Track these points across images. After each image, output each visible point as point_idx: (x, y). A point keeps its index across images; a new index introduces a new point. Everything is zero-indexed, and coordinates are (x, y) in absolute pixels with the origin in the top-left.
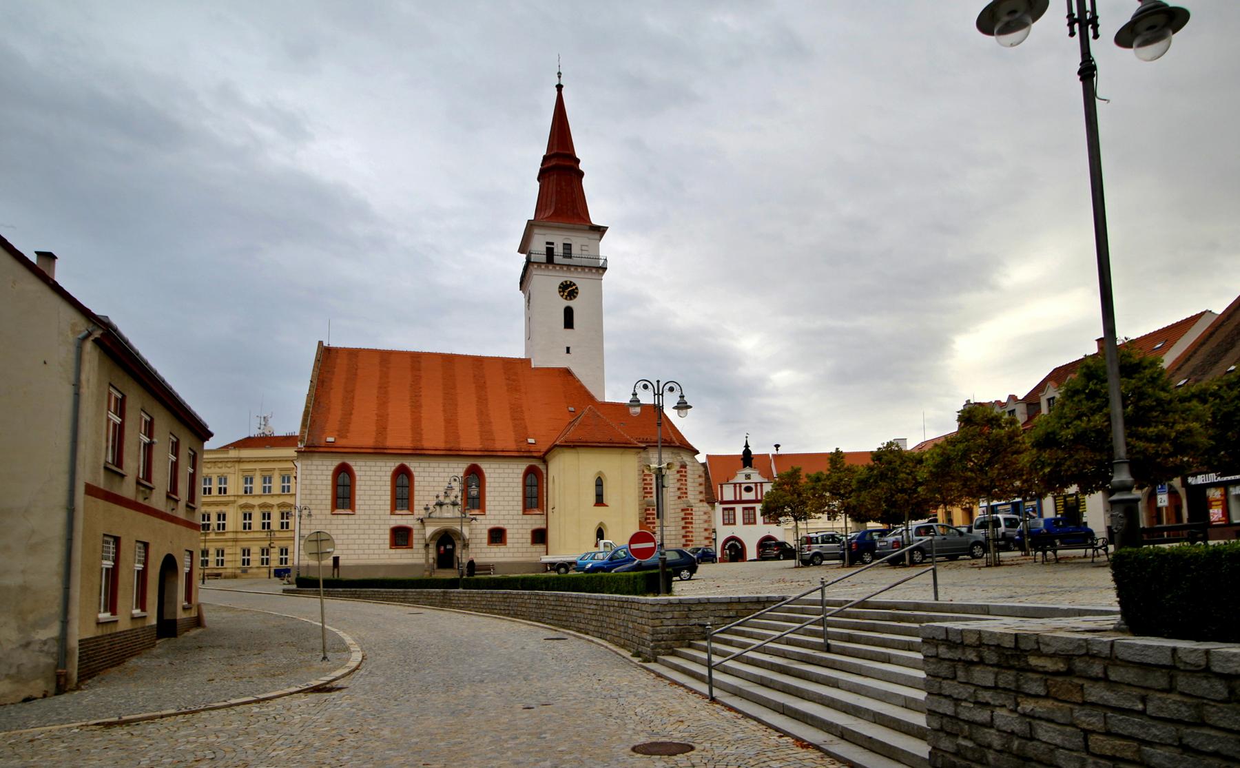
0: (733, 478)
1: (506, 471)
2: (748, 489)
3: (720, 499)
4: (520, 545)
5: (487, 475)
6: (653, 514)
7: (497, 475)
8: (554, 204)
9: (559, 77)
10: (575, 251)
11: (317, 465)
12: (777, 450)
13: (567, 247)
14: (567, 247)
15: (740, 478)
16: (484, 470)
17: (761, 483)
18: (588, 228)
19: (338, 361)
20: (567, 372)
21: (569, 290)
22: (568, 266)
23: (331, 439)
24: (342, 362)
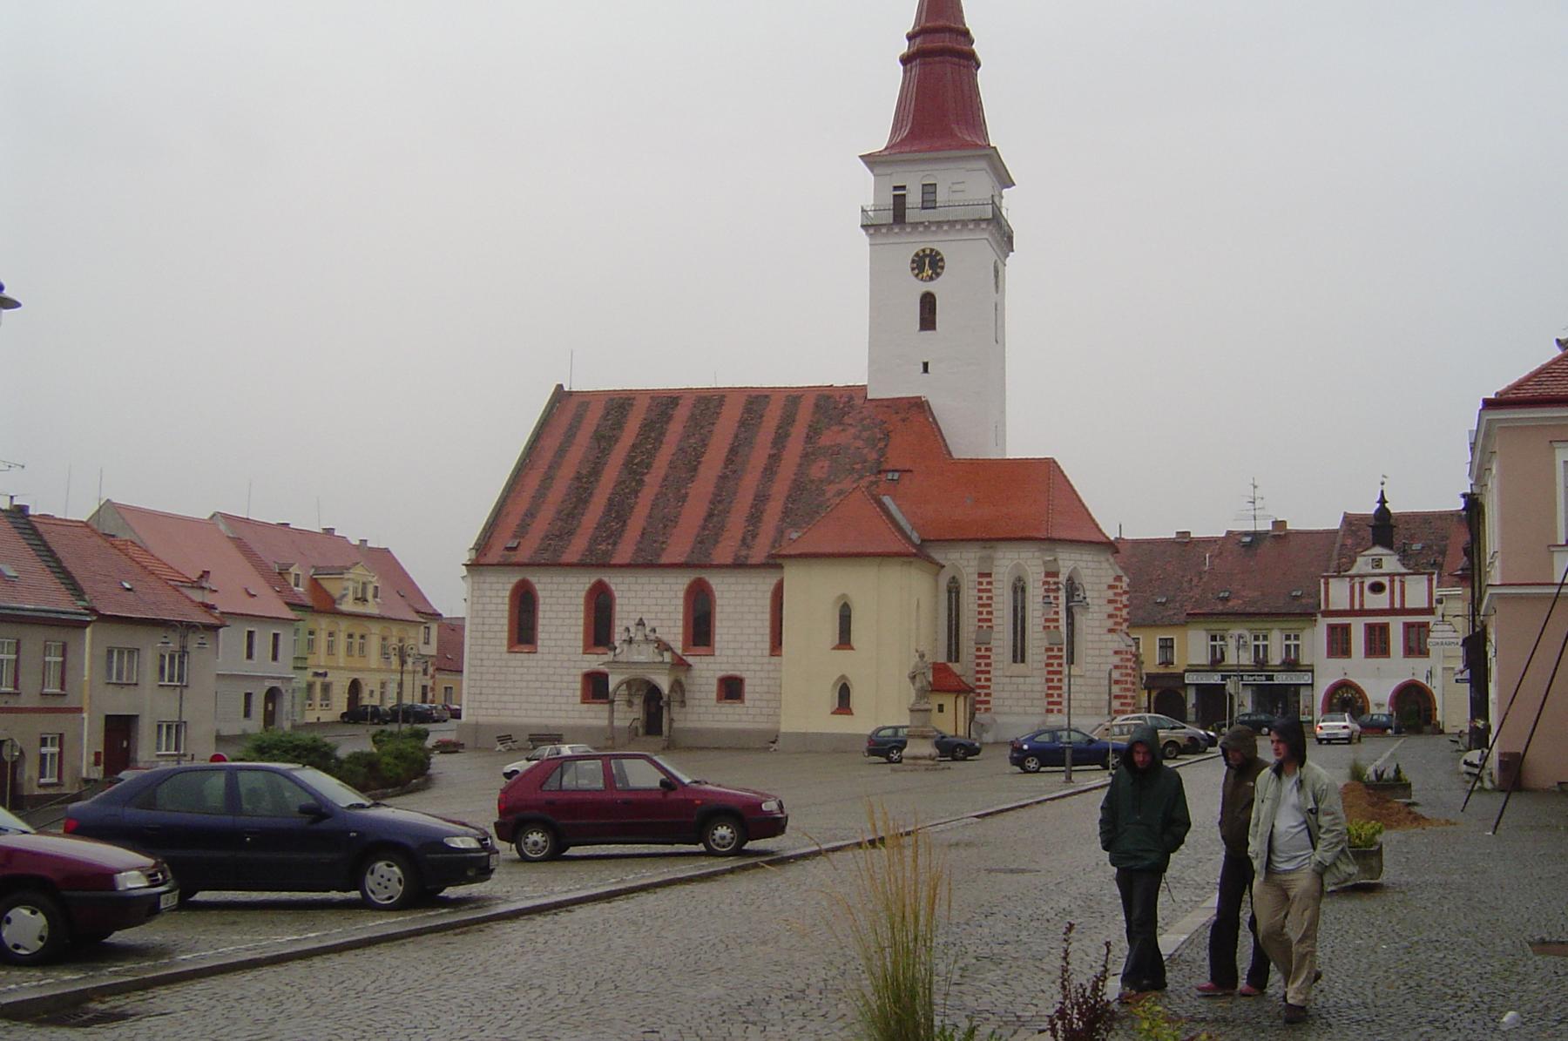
2: (1377, 588)
4: (764, 704)
10: (942, 196)
11: (491, 583)
13: (929, 190)
14: (929, 190)
15: (1362, 565)
16: (714, 587)
20: (918, 406)
21: (929, 264)
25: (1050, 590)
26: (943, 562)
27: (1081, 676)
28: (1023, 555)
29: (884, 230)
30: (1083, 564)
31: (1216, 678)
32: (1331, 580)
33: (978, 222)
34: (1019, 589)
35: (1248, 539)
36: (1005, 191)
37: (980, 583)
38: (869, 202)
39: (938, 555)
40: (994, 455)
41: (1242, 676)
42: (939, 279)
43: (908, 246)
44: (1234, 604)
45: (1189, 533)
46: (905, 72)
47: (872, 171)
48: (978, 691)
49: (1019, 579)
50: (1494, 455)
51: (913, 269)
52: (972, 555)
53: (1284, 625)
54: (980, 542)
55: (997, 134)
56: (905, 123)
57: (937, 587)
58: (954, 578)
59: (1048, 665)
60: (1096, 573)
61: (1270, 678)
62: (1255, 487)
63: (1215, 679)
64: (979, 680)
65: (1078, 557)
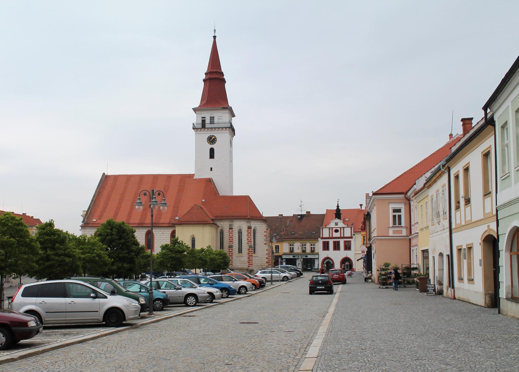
0: (328, 224)
2: (336, 231)
3: (321, 236)
5: (155, 235)
6: (252, 252)
7: (159, 235)
8: (206, 98)
9: (215, 32)
10: (216, 121)
12: (361, 207)
13: (212, 118)
14: (212, 118)
15: (332, 225)
17: (344, 228)
18: (221, 108)
19: (109, 182)
20: (209, 181)
21: (212, 140)
22: (212, 128)
23: (94, 220)
24: (110, 182)
26: (219, 225)
27: (257, 257)
28: (241, 223)
29: (199, 130)
30: (258, 226)
31: (291, 256)
32: (323, 229)
33: (226, 128)
34: (240, 232)
35: (299, 217)
37: (230, 231)
40: (228, 194)
41: (299, 256)
42: (215, 144)
43: (205, 135)
44: (297, 235)
45: (282, 215)
47: (195, 113)
49: (240, 230)
50: (375, 206)
52: (227, 223)
53: (310, 242)
54: (229, 220)
55: (232, 101)
56: (205, 99)
57: (217, 232)
58: (222, 229)
59: (248, 254)
60: (261, 228)
61: (307, 256)
62: (301, 202)
63: (291, 257)
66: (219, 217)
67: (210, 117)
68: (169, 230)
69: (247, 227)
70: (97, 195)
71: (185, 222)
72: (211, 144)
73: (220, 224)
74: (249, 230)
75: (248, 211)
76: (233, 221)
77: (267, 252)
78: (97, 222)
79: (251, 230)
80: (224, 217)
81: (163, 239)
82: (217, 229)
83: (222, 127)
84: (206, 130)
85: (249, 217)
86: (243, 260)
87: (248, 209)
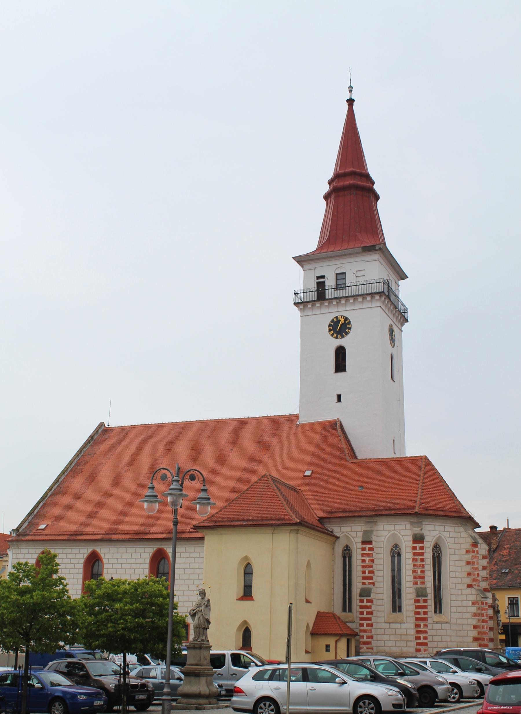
1: (193, 555)
9: (351, 91)
10: (349, 280)
13: (340, 276)
14: (340, 276)
18: (360, 250)
19: (107, 441)
22: (339, 299)
23: (42, 527)
25: (418, 555)
26: (338, 535)
28: (397, 527)
30: (446, 534)
33: (372, 294)
36: (401, 282)
38: (300, 287)
39: (337, 529)
46: (327, 205)
47: (302, 267)
48: (362, 634)
49: (396, 546)
51: (330, 331)
54: (364, 519)
58: (347, 546)
64: (361, 625)
65: (442, 528)
66: (338, 512)
67: (337, 274)
68: (147, 550)
69: (410, 538)
70: (71, 470)
71: (224, 521)
72: (337, 337)
73: (342, 530)
74: (418, 546)
75: (419, 494)
76: (375, 523)
77: (474, 609)
78: (47, 531)
79: (421, 545)
80: (351, 511)
81: (192, 571)
82: (334, 543)
83: (363, 295)
84: (326, 304)
85: (416, 510)
86: (404, 631)
87: (420, 490)
